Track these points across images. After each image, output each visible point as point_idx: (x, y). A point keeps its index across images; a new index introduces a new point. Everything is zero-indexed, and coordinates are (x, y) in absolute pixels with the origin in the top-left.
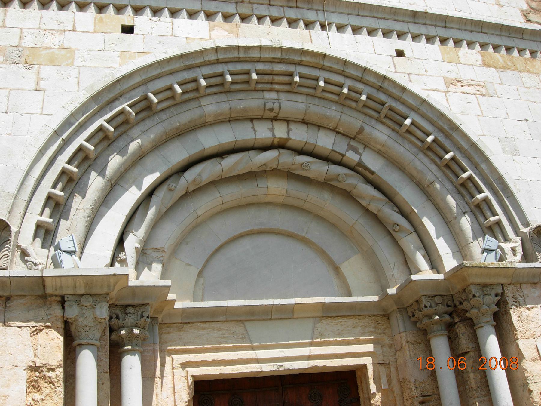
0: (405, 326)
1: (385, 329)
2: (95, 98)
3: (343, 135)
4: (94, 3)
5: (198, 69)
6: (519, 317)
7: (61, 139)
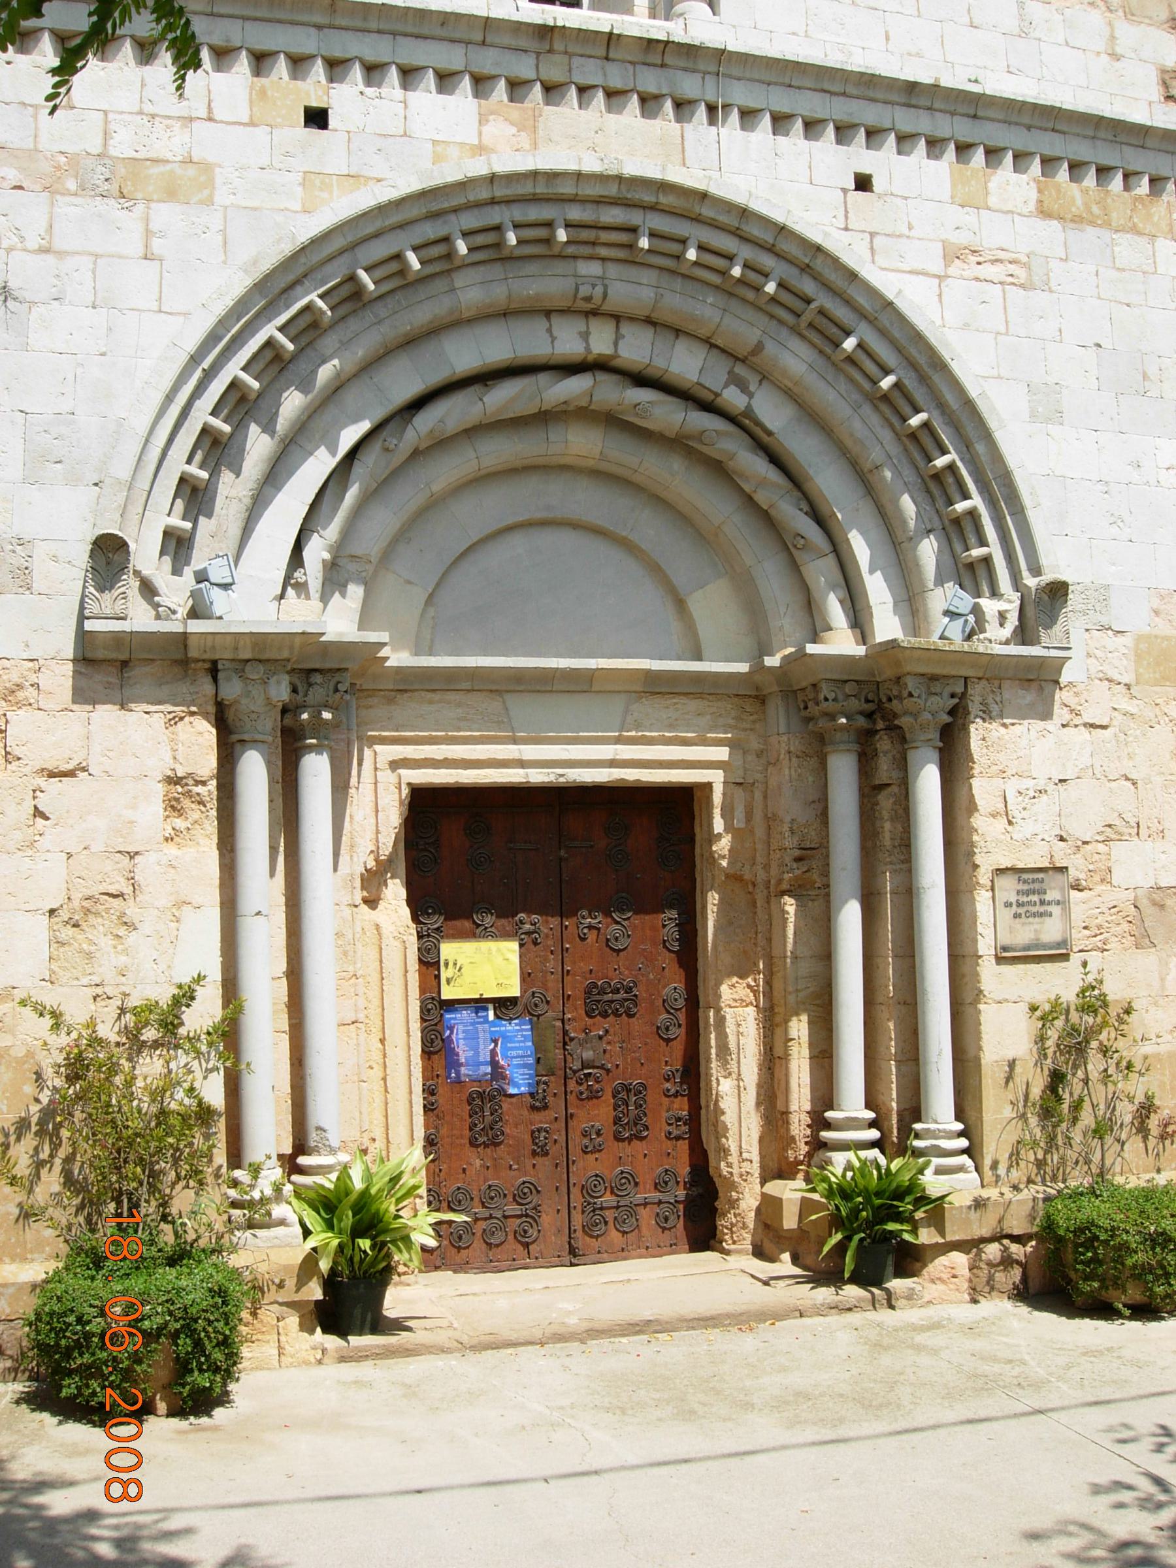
0: (788, 725)
1: (754, 722)
2: (259, 287)
3: (723, 351)
4: (248, 50)
5: (453, 217)
6: (984, 739)
7: (200, 369)
